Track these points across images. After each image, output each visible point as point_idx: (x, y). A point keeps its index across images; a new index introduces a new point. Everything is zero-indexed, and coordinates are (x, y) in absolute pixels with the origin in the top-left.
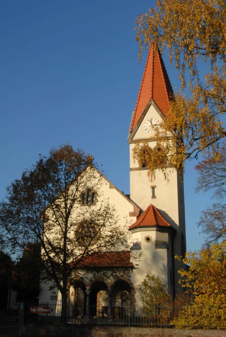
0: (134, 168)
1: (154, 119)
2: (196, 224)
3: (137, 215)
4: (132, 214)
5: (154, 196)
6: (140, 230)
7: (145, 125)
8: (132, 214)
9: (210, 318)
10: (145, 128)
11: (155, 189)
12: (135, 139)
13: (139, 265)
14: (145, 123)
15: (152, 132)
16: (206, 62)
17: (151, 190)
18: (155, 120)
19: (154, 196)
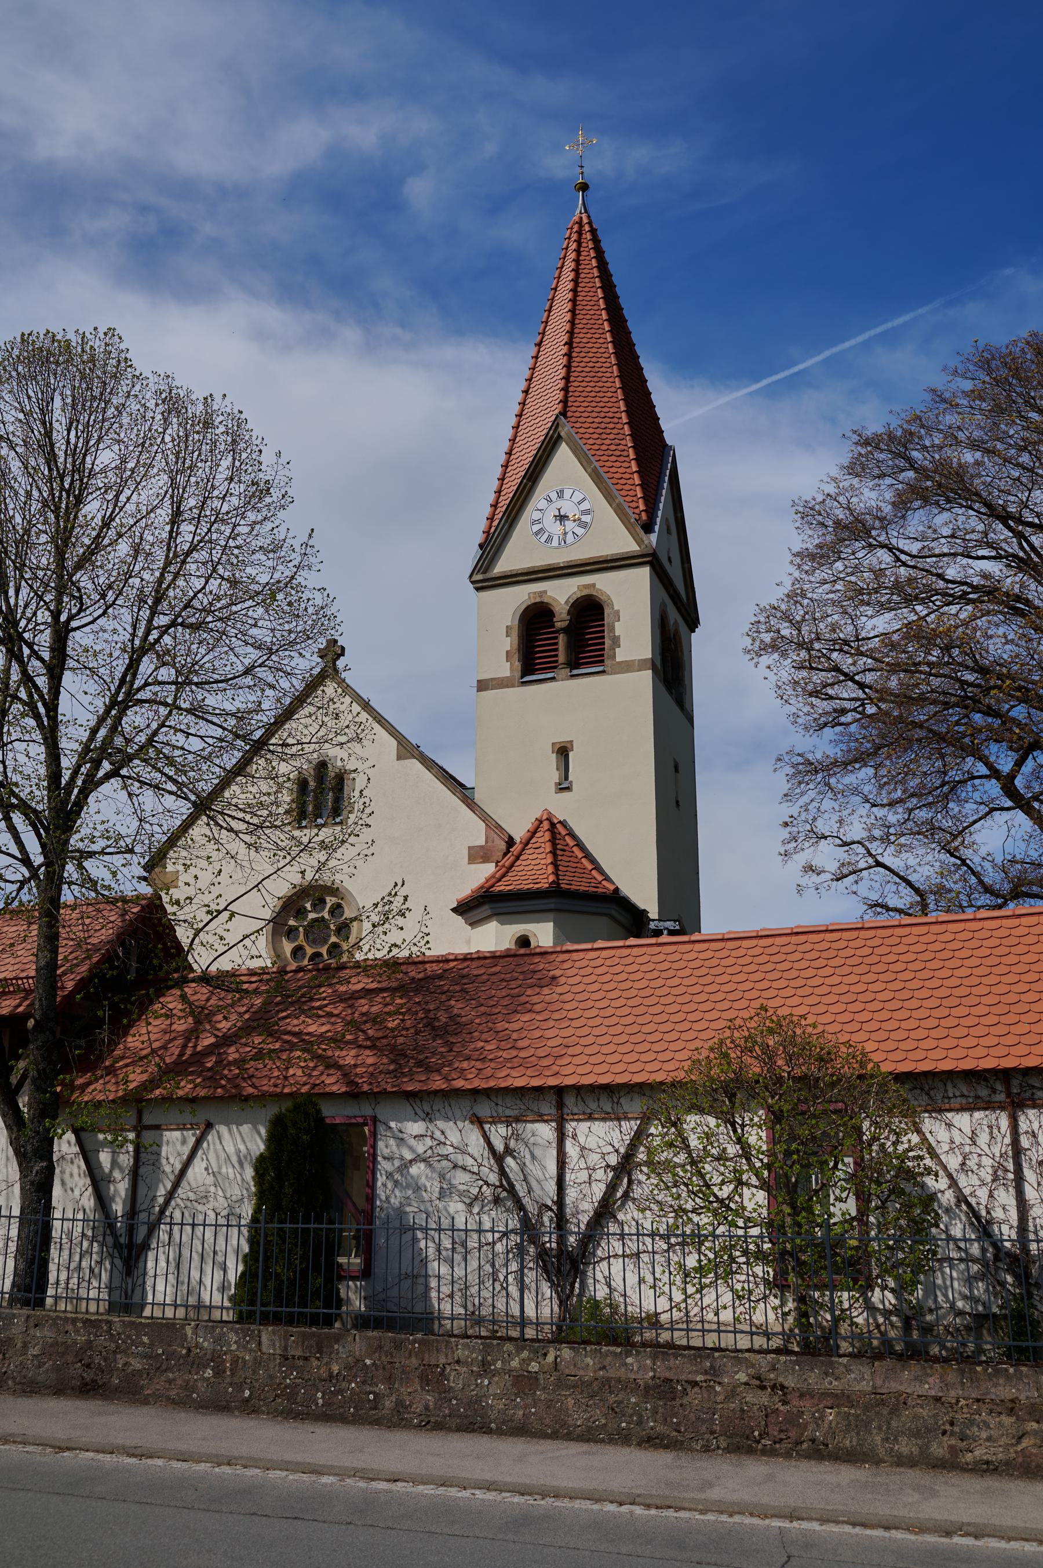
4: (477, 855)
5: (564, 787)
8: (477, 855)
19: (564, 787)
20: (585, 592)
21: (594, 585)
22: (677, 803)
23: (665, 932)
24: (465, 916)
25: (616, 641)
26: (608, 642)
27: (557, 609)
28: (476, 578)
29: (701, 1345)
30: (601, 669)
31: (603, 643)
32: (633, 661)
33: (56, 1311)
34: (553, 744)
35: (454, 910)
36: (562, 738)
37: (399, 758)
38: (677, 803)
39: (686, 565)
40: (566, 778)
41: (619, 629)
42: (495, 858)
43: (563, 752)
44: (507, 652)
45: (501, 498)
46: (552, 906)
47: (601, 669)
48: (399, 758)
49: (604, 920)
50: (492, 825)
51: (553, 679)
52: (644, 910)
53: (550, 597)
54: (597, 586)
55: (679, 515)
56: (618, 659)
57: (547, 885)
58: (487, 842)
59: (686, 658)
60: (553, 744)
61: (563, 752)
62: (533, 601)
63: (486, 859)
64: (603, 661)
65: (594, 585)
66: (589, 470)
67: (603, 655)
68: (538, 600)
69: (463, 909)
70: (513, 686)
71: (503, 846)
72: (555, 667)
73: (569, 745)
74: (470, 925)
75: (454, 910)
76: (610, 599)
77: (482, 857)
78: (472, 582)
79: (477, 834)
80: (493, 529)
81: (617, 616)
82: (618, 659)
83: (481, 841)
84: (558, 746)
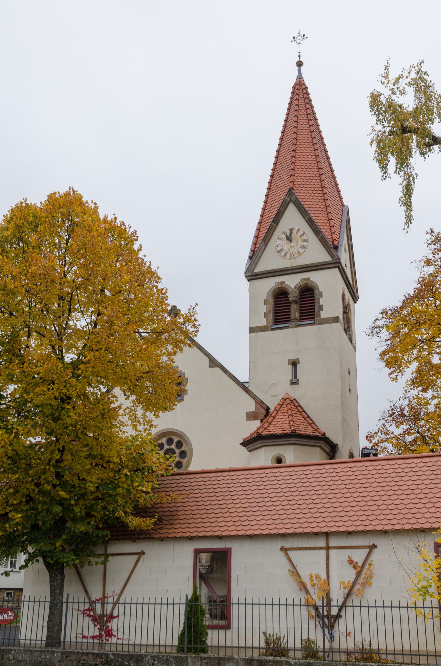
0: (257, 327)
1: (297, 229)
2: (371, 145)
3: (262, 416)
4: (251, 416)
5: (294, 382)
6: (264, 444)
7: (279, 242)
8: (251, 416)
9: (94, 388)
10: (279, 248)
11: (298, 366)
12: (258, 271)
13: (349, 557)
14: (279, 239)
15: (291, 256)
16: (390, 178)
17: (290, 367)
18: (297, 232)
19: (294, 382)
20: (304, 282)
21: (309, 279)
22: (350, 391)
23: (372, 455)
24: (247, 447)
25: (321, 308)
26: (316, 308)
27: (290, 291)
28: (247, 275)
29: (402, 662)
30: (312, 322)
31: (314, 309)
32: (330, 318)
33: (122, 651)
34: (289, 360)
35: (242, 444)
36: (293, 357)
37: (210, 367)
38: (350, 391)
39: (353, 269)
40: (296, 377)
41: (322, 301)
42: (260, 418)
43: (294, 364)
44: (265, 313)
45: (260, 233)
46: (261, 445)
47: (312, 322)
48: (210, 367)
49: (318, 449)
50: (258, 402)
51: (288, 327)
52: (337, 444)
53: (286, 285)
54: (311, 279)
55: (350, 242)
56: (322, 317)
57: (290, 432)
58: (256, 409)
59: (352, 316)
60: (289, 360)
61: (294, 364)
62: (277, 287)
63: (255, 418)
64: (314, 318)
65: (309, 279)
66: (306, 218)
67: (314, 315)
68: (280, 286)
69: (246, 443)
70: (268, 331)
71: (264, 412)
72: (289, 321)
73: (297, 361)
74: (250, 451)
75: (242, 444)
76: (317, 285)
77: (253, 417)
78: (246, 277)
79: (251, 406)
80: (256, 249)
81: (321, 294)
82: (322, 317)
83: (253, 410)
84: (291, 361)
